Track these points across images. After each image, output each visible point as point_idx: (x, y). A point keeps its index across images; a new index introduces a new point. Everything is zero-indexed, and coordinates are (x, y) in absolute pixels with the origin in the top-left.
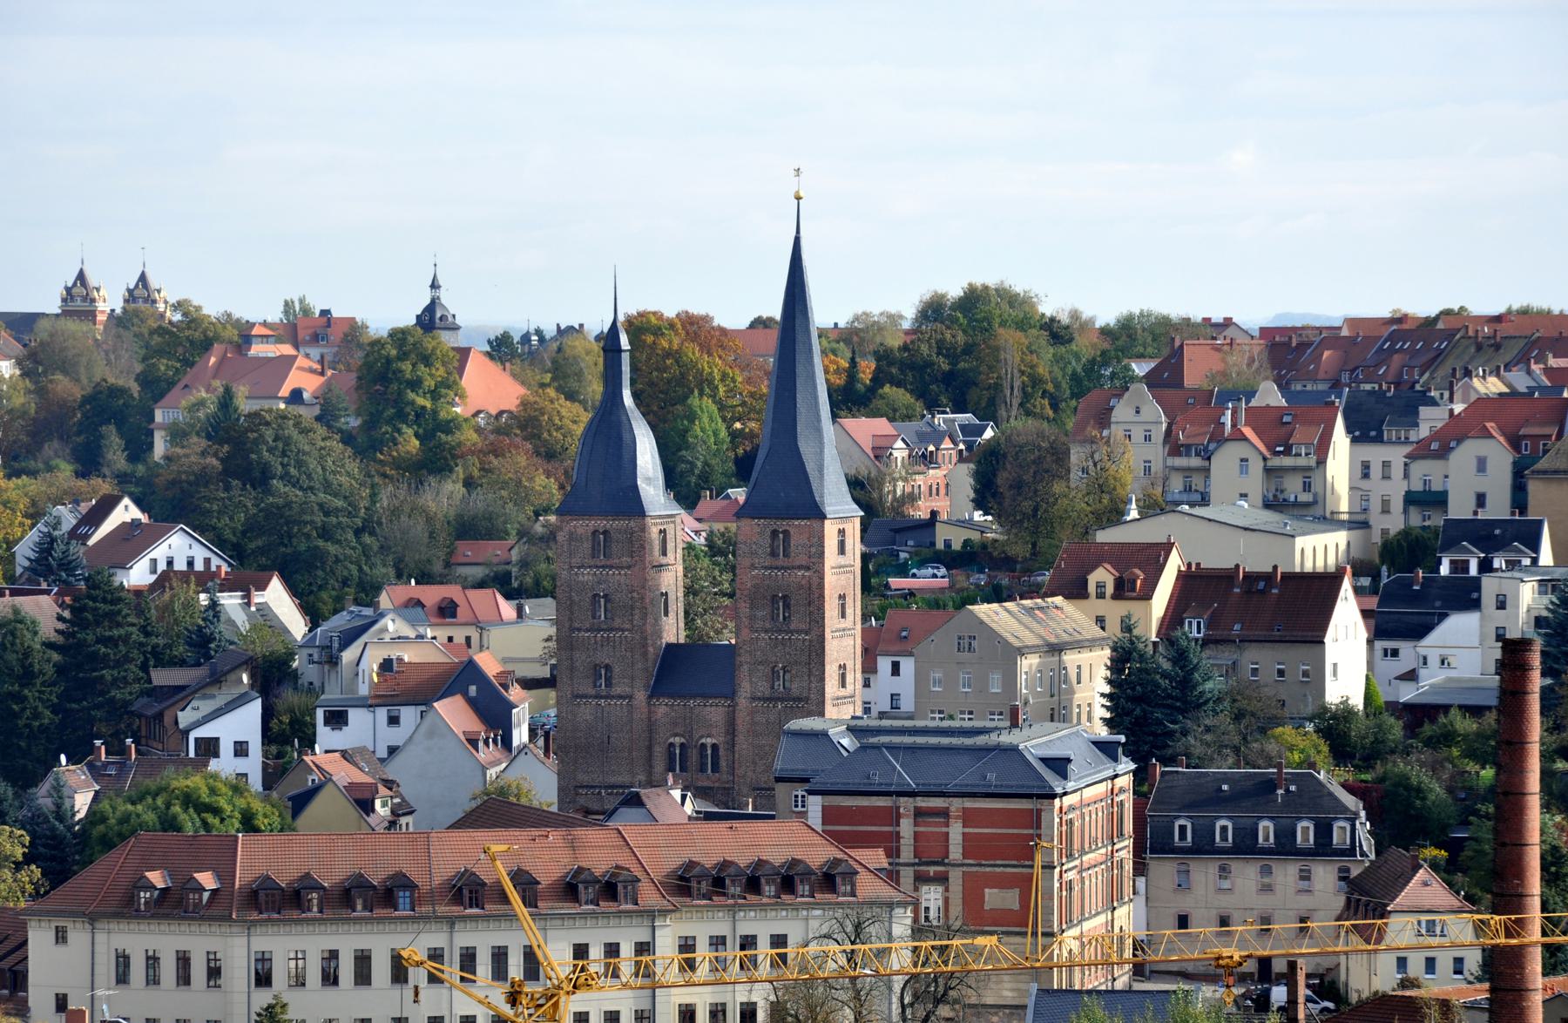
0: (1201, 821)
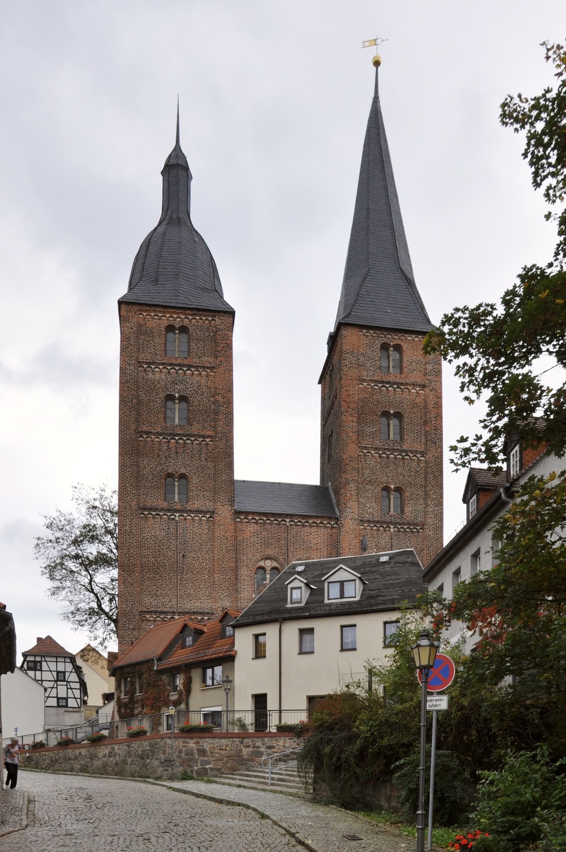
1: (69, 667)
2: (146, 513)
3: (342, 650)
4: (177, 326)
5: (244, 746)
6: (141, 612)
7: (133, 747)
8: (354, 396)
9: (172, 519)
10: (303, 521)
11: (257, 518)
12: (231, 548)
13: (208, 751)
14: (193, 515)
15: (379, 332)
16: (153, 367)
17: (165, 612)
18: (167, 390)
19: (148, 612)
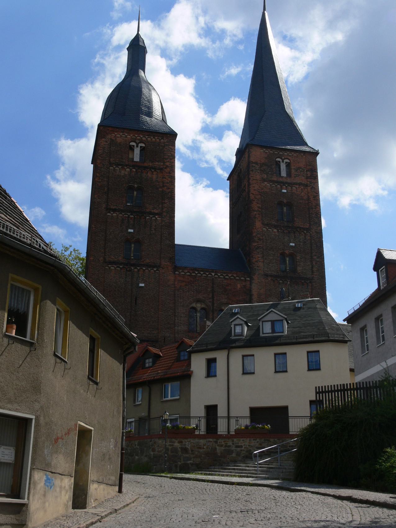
3: (244, 373)
5: (218, 445)
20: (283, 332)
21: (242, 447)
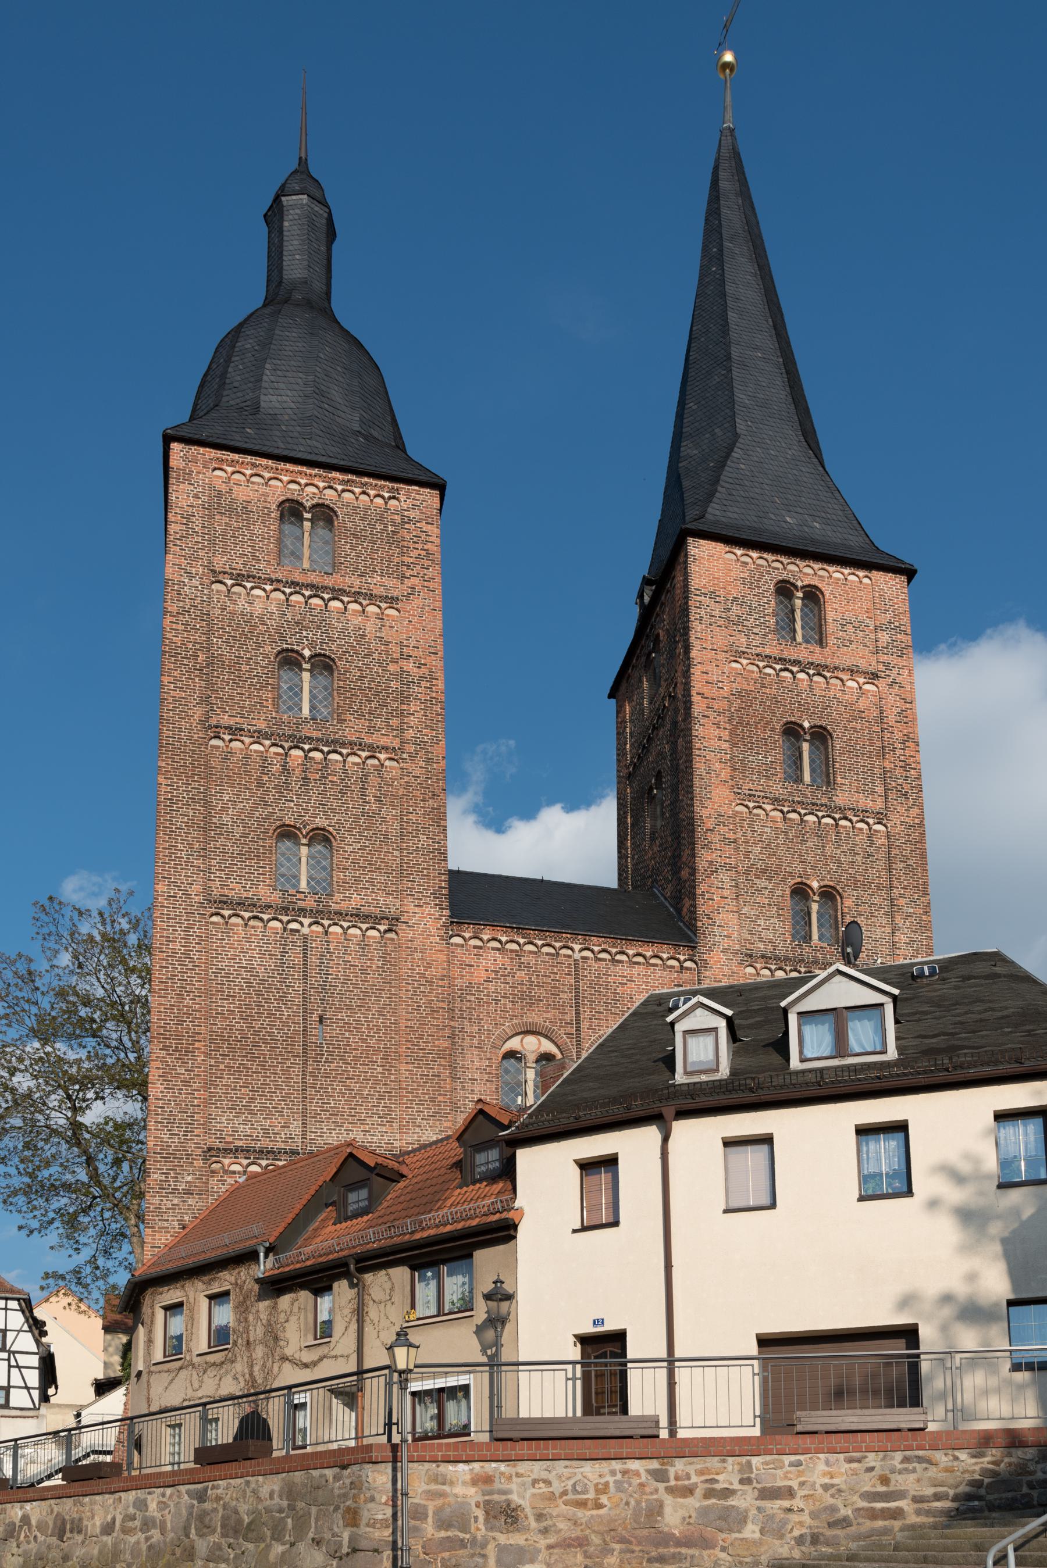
0: (1018, 1354)
1: (17, 1320)
2: (226, 913)
4: (308, 504)
5: (670, 1490)
6: (210, 1149)
7: (218, 1498)
8: (720, 685)
9: (292, 930)
10: (614, 950)
11: (504, 939)
12: (441, 1005)
13: (528, 1511)
14: (345, 925)
15: (770, 557)
16: (249, 585)
17: (271, 1152)
18: (283, 639)
19: (227, 1151)
20: (884, 1052)
21: (790, 1493)
